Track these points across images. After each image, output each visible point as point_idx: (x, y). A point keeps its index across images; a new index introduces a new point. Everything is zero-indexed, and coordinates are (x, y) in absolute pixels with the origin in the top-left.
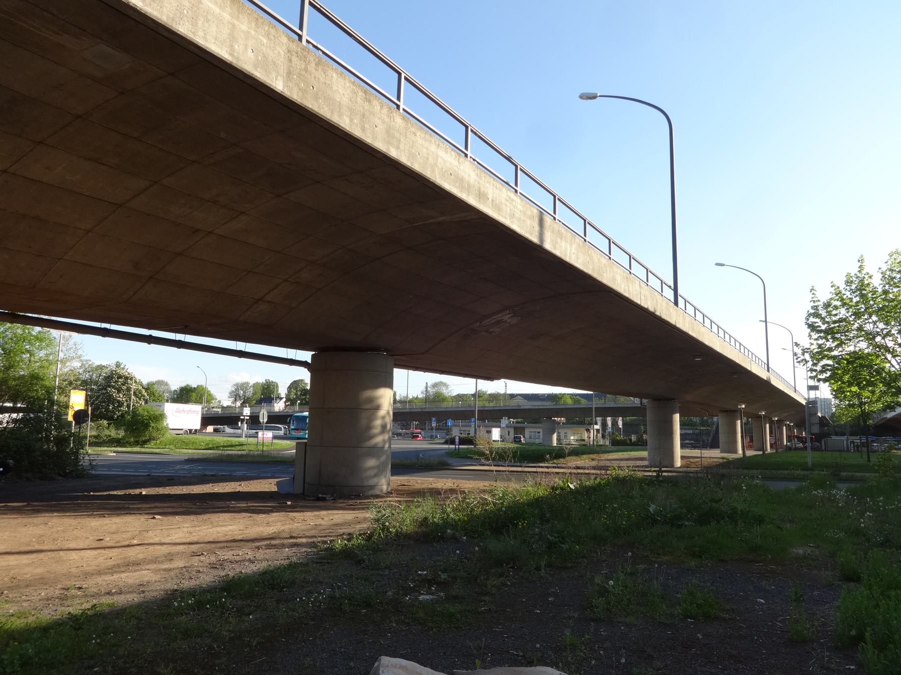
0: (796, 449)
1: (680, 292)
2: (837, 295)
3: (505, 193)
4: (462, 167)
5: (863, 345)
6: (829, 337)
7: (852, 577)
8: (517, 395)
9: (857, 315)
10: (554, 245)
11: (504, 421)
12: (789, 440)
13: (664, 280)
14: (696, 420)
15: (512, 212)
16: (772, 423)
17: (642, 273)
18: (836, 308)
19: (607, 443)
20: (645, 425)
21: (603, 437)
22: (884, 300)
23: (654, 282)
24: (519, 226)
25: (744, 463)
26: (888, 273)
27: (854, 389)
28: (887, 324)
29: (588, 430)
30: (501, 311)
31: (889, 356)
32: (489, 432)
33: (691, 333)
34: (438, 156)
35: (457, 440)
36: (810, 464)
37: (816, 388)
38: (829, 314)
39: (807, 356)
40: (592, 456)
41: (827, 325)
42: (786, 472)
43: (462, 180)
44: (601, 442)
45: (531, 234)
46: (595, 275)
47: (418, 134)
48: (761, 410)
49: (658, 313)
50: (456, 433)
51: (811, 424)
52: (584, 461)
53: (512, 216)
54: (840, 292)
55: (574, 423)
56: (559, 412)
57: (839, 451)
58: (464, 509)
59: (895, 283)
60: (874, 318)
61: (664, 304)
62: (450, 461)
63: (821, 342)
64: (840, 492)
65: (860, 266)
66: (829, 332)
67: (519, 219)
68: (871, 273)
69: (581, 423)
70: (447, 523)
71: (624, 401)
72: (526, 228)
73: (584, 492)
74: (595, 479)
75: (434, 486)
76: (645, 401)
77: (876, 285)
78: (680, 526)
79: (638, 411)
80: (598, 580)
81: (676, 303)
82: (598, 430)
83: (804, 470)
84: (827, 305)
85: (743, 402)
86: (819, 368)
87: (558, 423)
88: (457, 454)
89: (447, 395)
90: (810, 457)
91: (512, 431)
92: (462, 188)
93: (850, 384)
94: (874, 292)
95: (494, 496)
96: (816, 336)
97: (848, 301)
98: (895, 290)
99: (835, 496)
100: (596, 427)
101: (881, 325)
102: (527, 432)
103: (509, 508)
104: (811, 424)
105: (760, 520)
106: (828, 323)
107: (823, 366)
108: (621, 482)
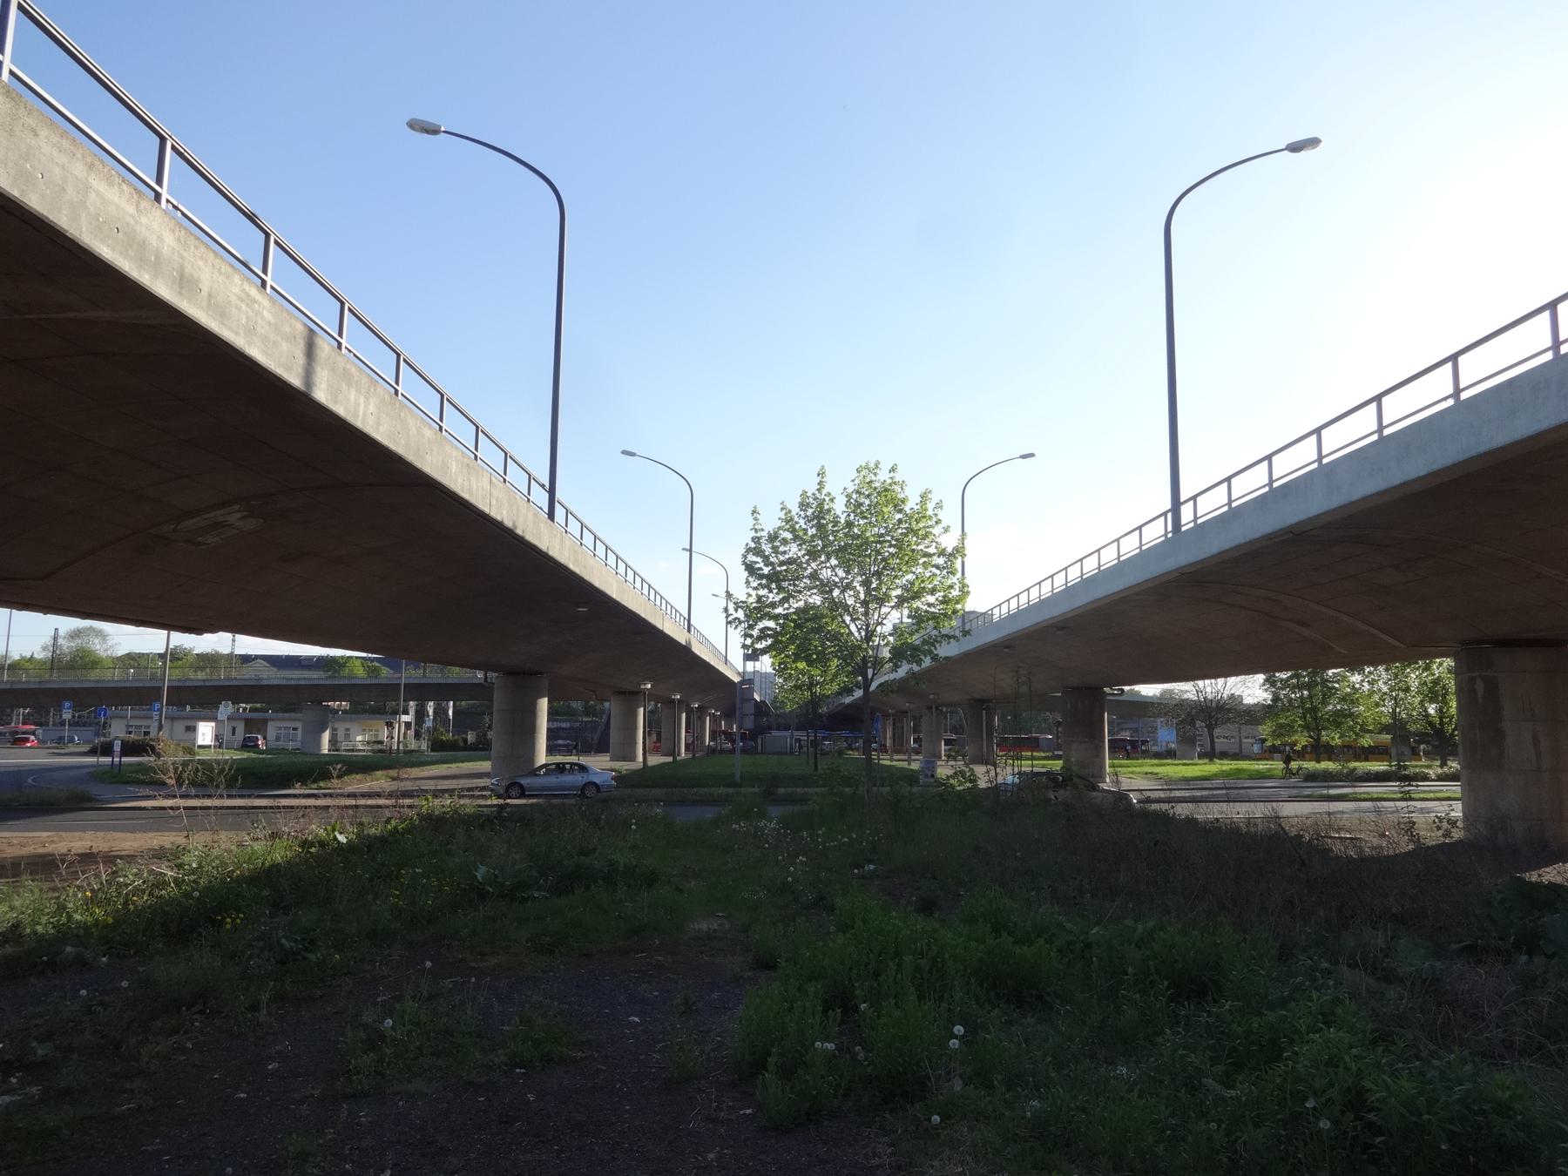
0: (722, 751)
1: (558, 495)
3: (237, 286)
4: (144, 220)
7: (766, 964)
8: (257, 657)
9: (813, 555)
10: (335, 393)
11: (226, 709)
12: (713, 738)
13: (534, 473)
14: (577, 705)
15: (250, 319)
16: (690, 712)
17: (496, 460)
18: (785, 542)
19: (424, 747)
20: (491, 714)
21: (417, 735)
22: (846, 535)
23: (516, 477)
24: (265, 352)
25: (644, 778)
27: (802, 665)
29: (390, 725)
30: (222, 505)
31: (847, 619)
32: (192, 729)
33: (571, 567)
34: (88, 188)
35: (117, 747)
38: (775, 550)
40: (393, 773)
41: (769, 567)
42: (703, 790)
43: (143, 245)
44: (413, 745)
45: (288, 369)
46: (410, 457)
47: (43, 133)
48: (674, 692)
49: (519, 532)
50: (118, 731)
51: (744, 715)
52: (380, 781)
53: (251, 331)
55: (365, 711)
56: (337, 692)
57: (780, 753)
58: (108, 900)
60: (834, 562)
61: (531, 517)
62: (96, 790)
67: (265, 339)
69: (378, 711)
70: (64, 934)
71: (457, 674)
72: (276, 354)
73: (366, 847)
74: (388, 821)
75: (50, 849)
76: (489, 674)
77: (839, 512)
78: (525, 900)
79: (480, 691)
80: (368, 1017)
81: (551, 515)
82: (408, 725)
83: (729, 786)
84: (773, 538)
85: (650, 680)
86: (755, 633)
87: (335, 712)
88: (118, 778)
89: (103, 654)
90: (739, 764)
91: (240, 728)
92: (141, 261)
93: (797, 658)
94: (836, 523)
95: (180, 866)
96: (755, 584)
99: (763, 829)
100: (405, 718)
102: (272, 729)
103: (209, 889)
104: (744, 715)
105: (651, 880)
106: (772, 564)
107: (762, 630)
108: (435, 823)
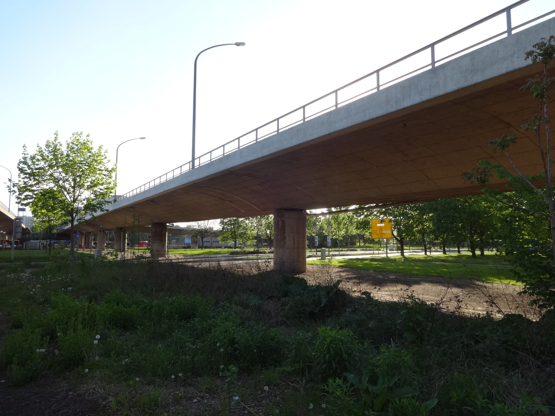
0: (6, 249)
2: (40, 152)
5: (52, 185)
6: (32, 178)
7: (18, 326)
18: (38, 160)
26: (71, 144)
27: (44, 211)
28: (66, 174)
31: (65, 193)
36: (12, 258)
37: (23, 210)
38: (34, 163)
39: (16, 189)
41: (30, 170)
51: (16, 233)
54: (42, 151)
59: (74, 151)
60: (60, 170)
63: (26, 180)
64: (26, 274)
65: (56, 138)
66: (32, 175)
68: (61, 143)
77: (63, 150)
83: (8, 262)
84: (33, 158)
86: (23, 197)
93: (42, 208)
94: (62, 155)
97: (46, 158)
98: (74, 155)
101: (64, 175)
106: (32, 169)
107: (26, 196)
